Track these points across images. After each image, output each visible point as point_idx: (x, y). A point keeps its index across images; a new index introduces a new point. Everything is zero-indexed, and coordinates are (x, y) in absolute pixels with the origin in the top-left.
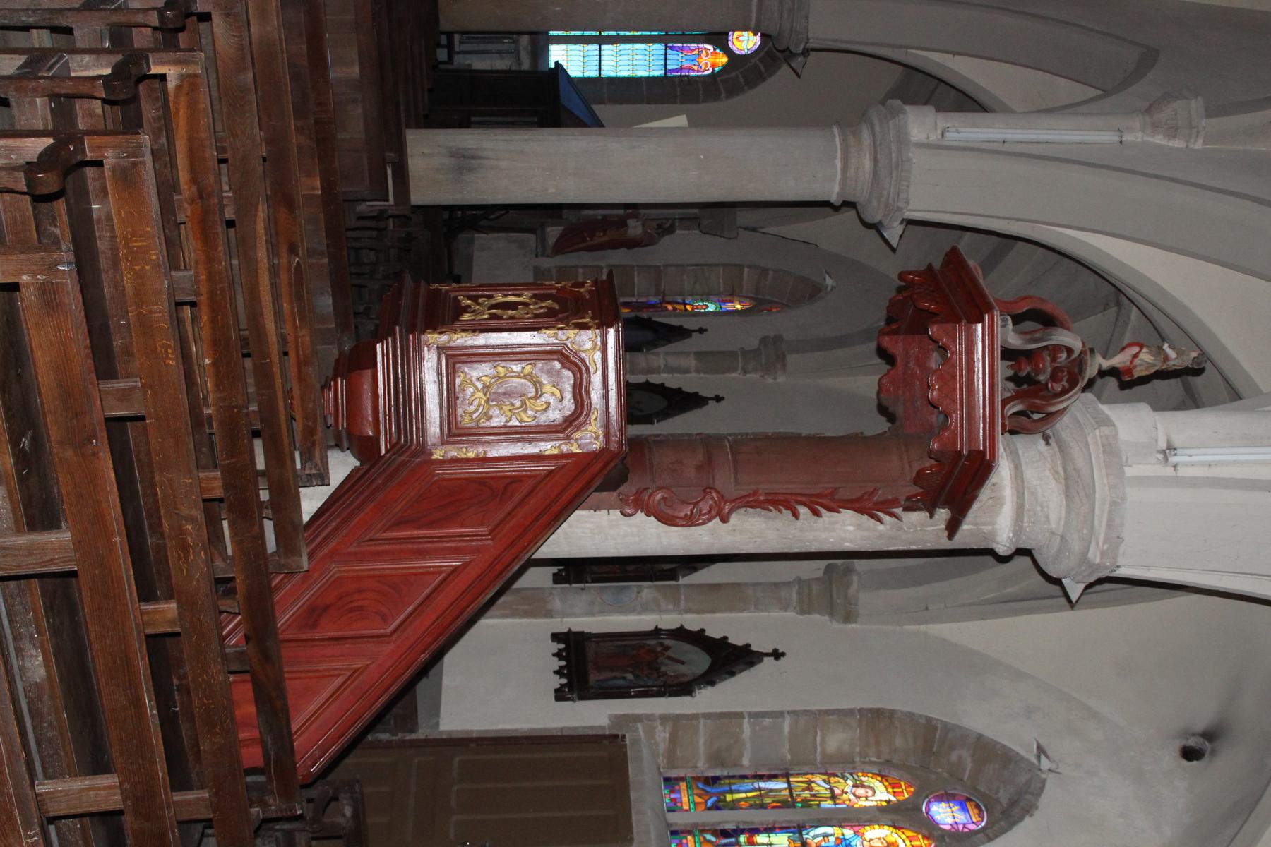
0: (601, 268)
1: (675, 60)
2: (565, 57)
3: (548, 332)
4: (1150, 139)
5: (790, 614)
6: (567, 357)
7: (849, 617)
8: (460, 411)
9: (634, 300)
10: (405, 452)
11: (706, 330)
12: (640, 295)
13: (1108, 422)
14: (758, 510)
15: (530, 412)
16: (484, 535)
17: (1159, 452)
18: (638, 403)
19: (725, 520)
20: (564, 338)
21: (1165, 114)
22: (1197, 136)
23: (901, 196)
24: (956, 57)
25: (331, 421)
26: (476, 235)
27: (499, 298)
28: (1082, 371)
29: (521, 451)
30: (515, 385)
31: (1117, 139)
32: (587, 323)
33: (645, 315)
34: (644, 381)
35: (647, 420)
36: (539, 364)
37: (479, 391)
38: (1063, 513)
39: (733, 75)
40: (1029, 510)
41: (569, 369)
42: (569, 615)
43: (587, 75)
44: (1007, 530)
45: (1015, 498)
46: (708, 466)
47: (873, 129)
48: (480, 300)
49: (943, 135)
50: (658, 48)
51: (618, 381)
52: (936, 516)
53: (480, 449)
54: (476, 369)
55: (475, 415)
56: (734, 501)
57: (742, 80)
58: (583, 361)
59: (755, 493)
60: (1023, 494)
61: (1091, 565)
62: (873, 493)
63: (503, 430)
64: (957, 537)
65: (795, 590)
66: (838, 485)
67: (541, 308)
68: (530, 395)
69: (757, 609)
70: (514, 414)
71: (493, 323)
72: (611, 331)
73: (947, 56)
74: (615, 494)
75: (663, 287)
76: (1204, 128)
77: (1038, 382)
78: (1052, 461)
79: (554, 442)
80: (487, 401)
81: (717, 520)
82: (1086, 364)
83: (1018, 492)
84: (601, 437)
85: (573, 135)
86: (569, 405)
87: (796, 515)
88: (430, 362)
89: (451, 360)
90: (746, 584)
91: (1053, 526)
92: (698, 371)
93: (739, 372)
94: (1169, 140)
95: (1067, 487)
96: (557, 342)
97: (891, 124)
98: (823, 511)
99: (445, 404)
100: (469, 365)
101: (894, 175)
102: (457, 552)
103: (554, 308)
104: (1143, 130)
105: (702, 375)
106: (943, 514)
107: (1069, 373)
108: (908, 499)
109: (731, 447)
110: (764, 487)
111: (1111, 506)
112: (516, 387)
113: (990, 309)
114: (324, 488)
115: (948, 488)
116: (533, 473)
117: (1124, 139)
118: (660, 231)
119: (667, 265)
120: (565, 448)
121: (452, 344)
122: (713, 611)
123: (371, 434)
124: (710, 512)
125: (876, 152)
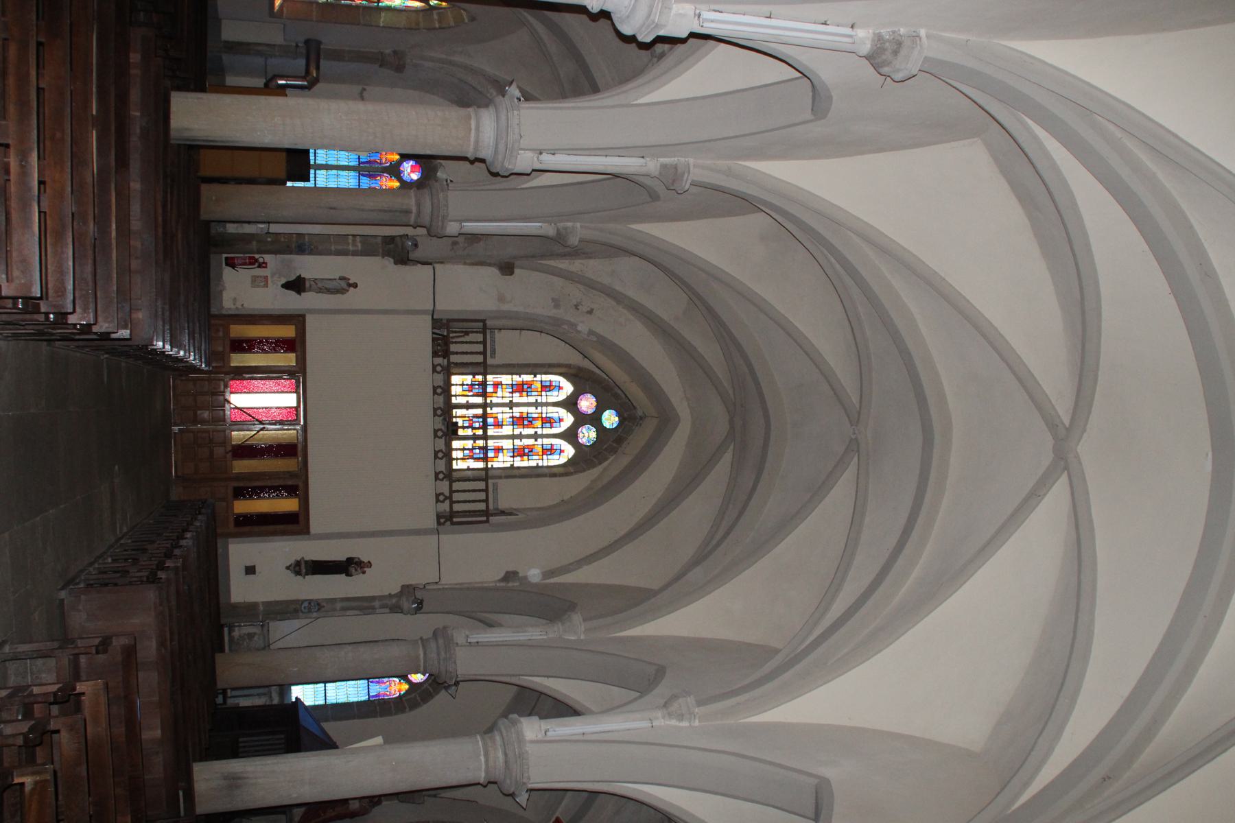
1: (376, 689)
4: (668, 723)
21: (675, 707)
22: (695, 718)
23: (525, 775)
24: (550, 679)
43: (317, 703)
50: (363, 683)
76: (697, 713)
101: (518, 762)
104: (663, 718)
117: (654, 724)
125: (505, 749)
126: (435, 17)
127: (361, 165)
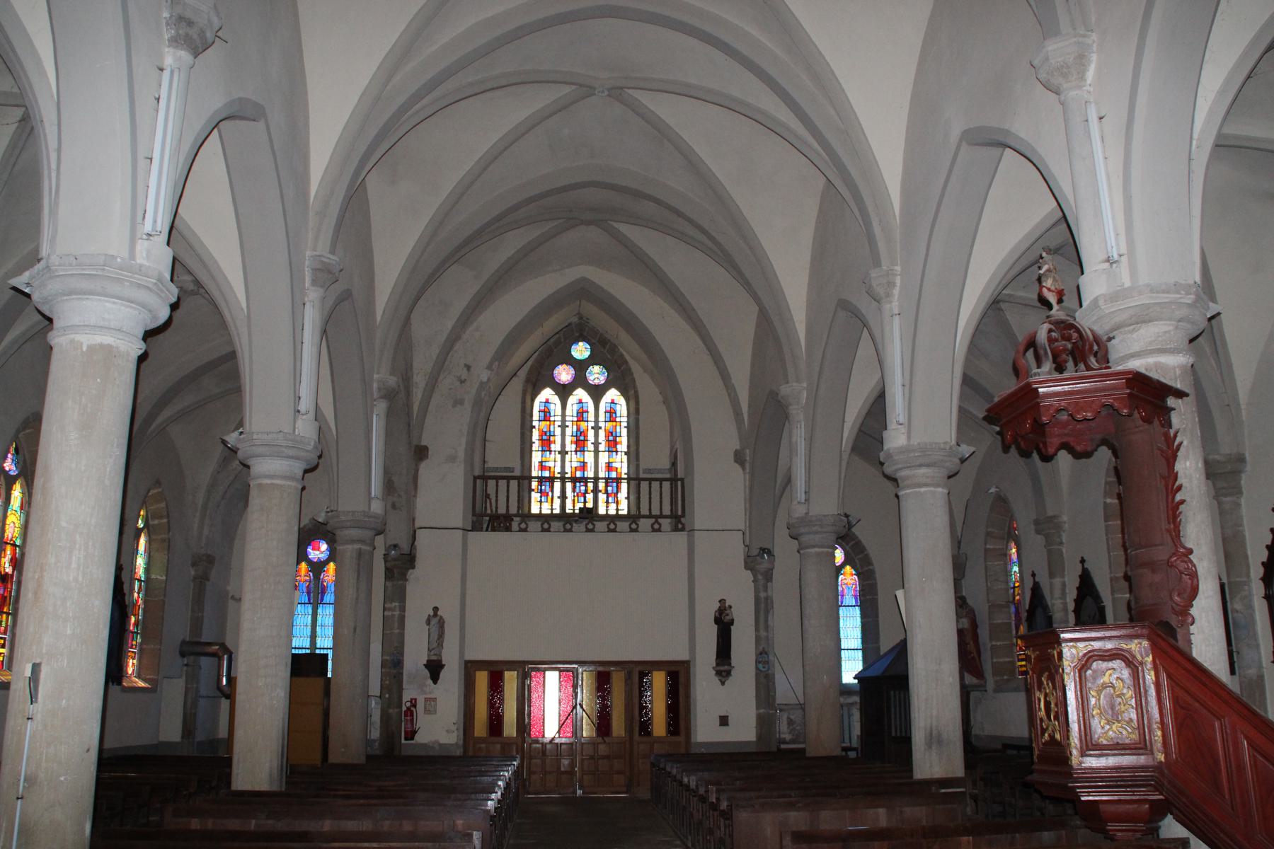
0: (992, 646)
1: (849, 599)
2: (850, 673)
3: (1066, 680)
4: (896, 297)
5: (1243, 501)
6: (1083, 666)
7: (1241, 459)
8: (1127, 741)
9: (1013, 623)
10: (1160, 781)
11: (1033, 572)
12: (1010, 618)
13: (1096, 300)
14: (1181, 528)
15: (1125, 691)
16: (1221, 723)
17: (1111, 267)
18: (1089, 617)
19: (1191, 551)
20: (1069, 668)
21: (881, 291)
25: (1138, 835)
26: (973, 733)
27: (1042, 713)
28: (1063, 322)
29: (1154, 697)
30: (1105, 702)
31: (897, 318)
32: (1058, 653)
33: (1024, 615)
34: (1073, 613)
35: (1102, 610)
36: (1089, 685)
37: (1112, 727)
38: (1162, 322)
39: (857, 561)
40: (1162, 345)
41: (1091, 664)
42: (1260, 662)
43: (861, 658)
44: (1178, 358)
45: (1154, 355)
46: (1152, 566)
47: (901, 469)
48: (1045, 727)
49: (901, 424)
50: (842, 611)
51: (1075, 631)
52: (1173, 406)
53: (1155, 726)
54: (1095, 729)
55: (1130, 730)
56: (1176, 545)
57: (860, 556)
58: (1085, 655)
59: (1168, 531)
60: (1150, 350)
61: (1196, 301)
62: (1159, 449)
63: (1139, 710)
64: (1187, 390)
65: (1224, 499)
66: (1158, 475)
67: (1048, 684)
68: (1112, 691)
69: (1241, 525)
70: (1127, 702)
71: (1062, 718)
72: (1062, 636)
73: (845, 426)
74: (1178, 630)
75: (1004, 603)
77: (1072, 347)
78: (1125, 333)
79: (1146, 674)
80: (1119, 722)
81: (1191, 557)
82: (1057, 319)
83: (1151, 353)
84: (1140, 641)
85: (913, 666)
86: (1117, 664)
87: (1182, 502)
88: (1092, 762)
89: (1090, 747)
90: (1223, 534)
91: (1171, 328)
92: (1063, 577)
93: (1061, 547)
94: (896, 286)
95: (1144, 322)
96: (1072, 673)
97: (896, 458)
98: (1177, 484)
99: (1123, 752)
100: (1093, 734)
101: (930, 453)
102: (1237, 744)
103: (1048, 675)
104: (891, 302)
105: (1066, 573)
106: (1171, 401)
107: (1065, 329)
108: (1163, 426)
109: (1136, 549)
110: (1164, 525)
111: (1154, 293)
112: (1107, 701)
113: (1029, 385)
114: (1192, 842)
115: (1152, 400)
116: (1170, 688)
118: (965, 607)
119: (988, 600)
120: (1149, 666)
121: (1079, 746)
122: (1246, 557)
123: (1147, 806)
124: (1186, 562)
126: (156, 522)
127: (312, 601)
